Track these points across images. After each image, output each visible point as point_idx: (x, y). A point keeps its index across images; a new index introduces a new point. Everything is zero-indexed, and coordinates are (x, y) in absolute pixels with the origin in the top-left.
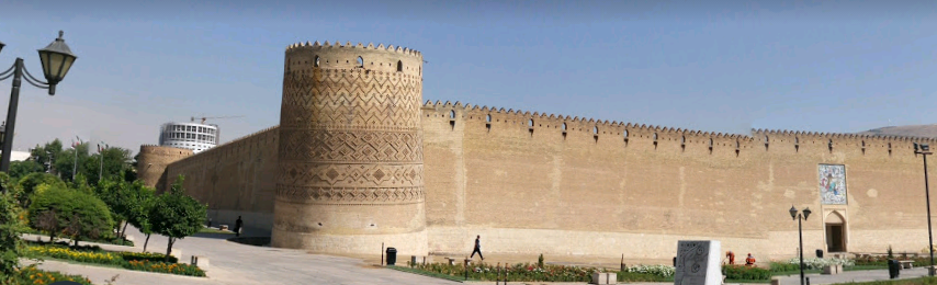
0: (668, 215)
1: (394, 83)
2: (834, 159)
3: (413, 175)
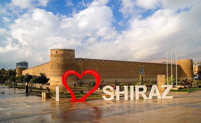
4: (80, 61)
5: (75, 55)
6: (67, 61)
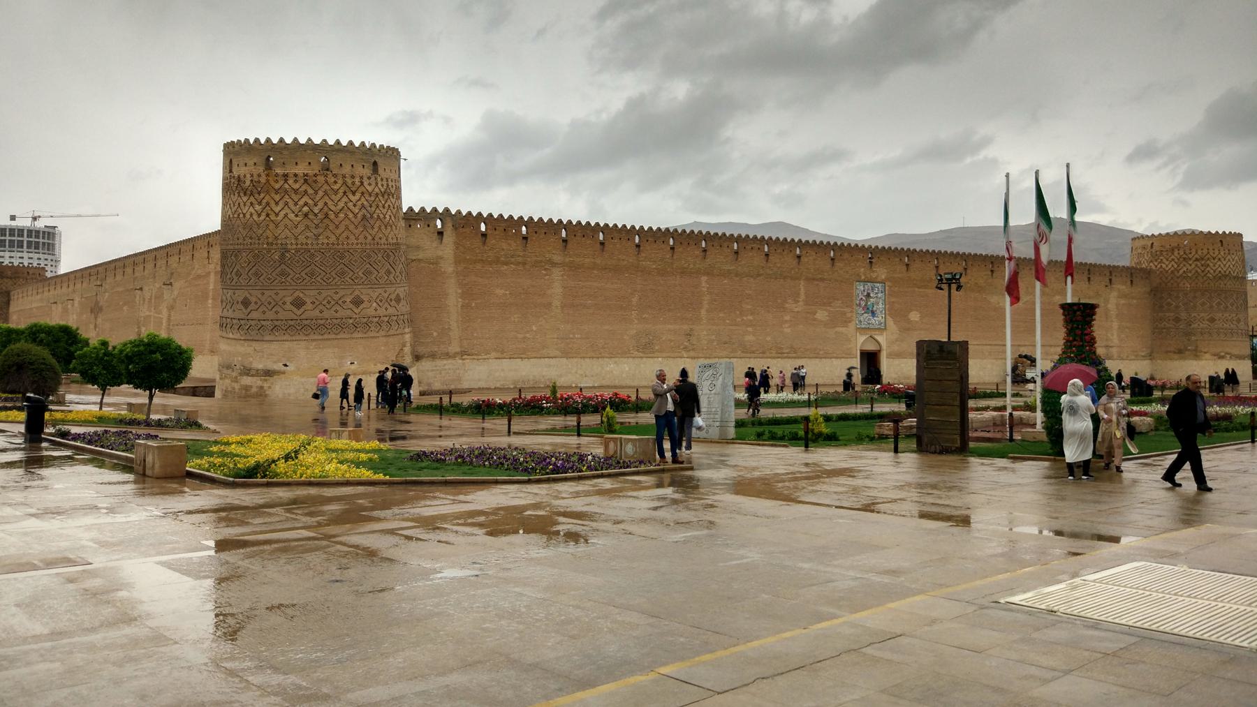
0: (689, 335)
1: (370, 189)
2: (874, 275)
3: (398, 300)
4: (440, 233)
5: (398, 189)
6: (342, 228)
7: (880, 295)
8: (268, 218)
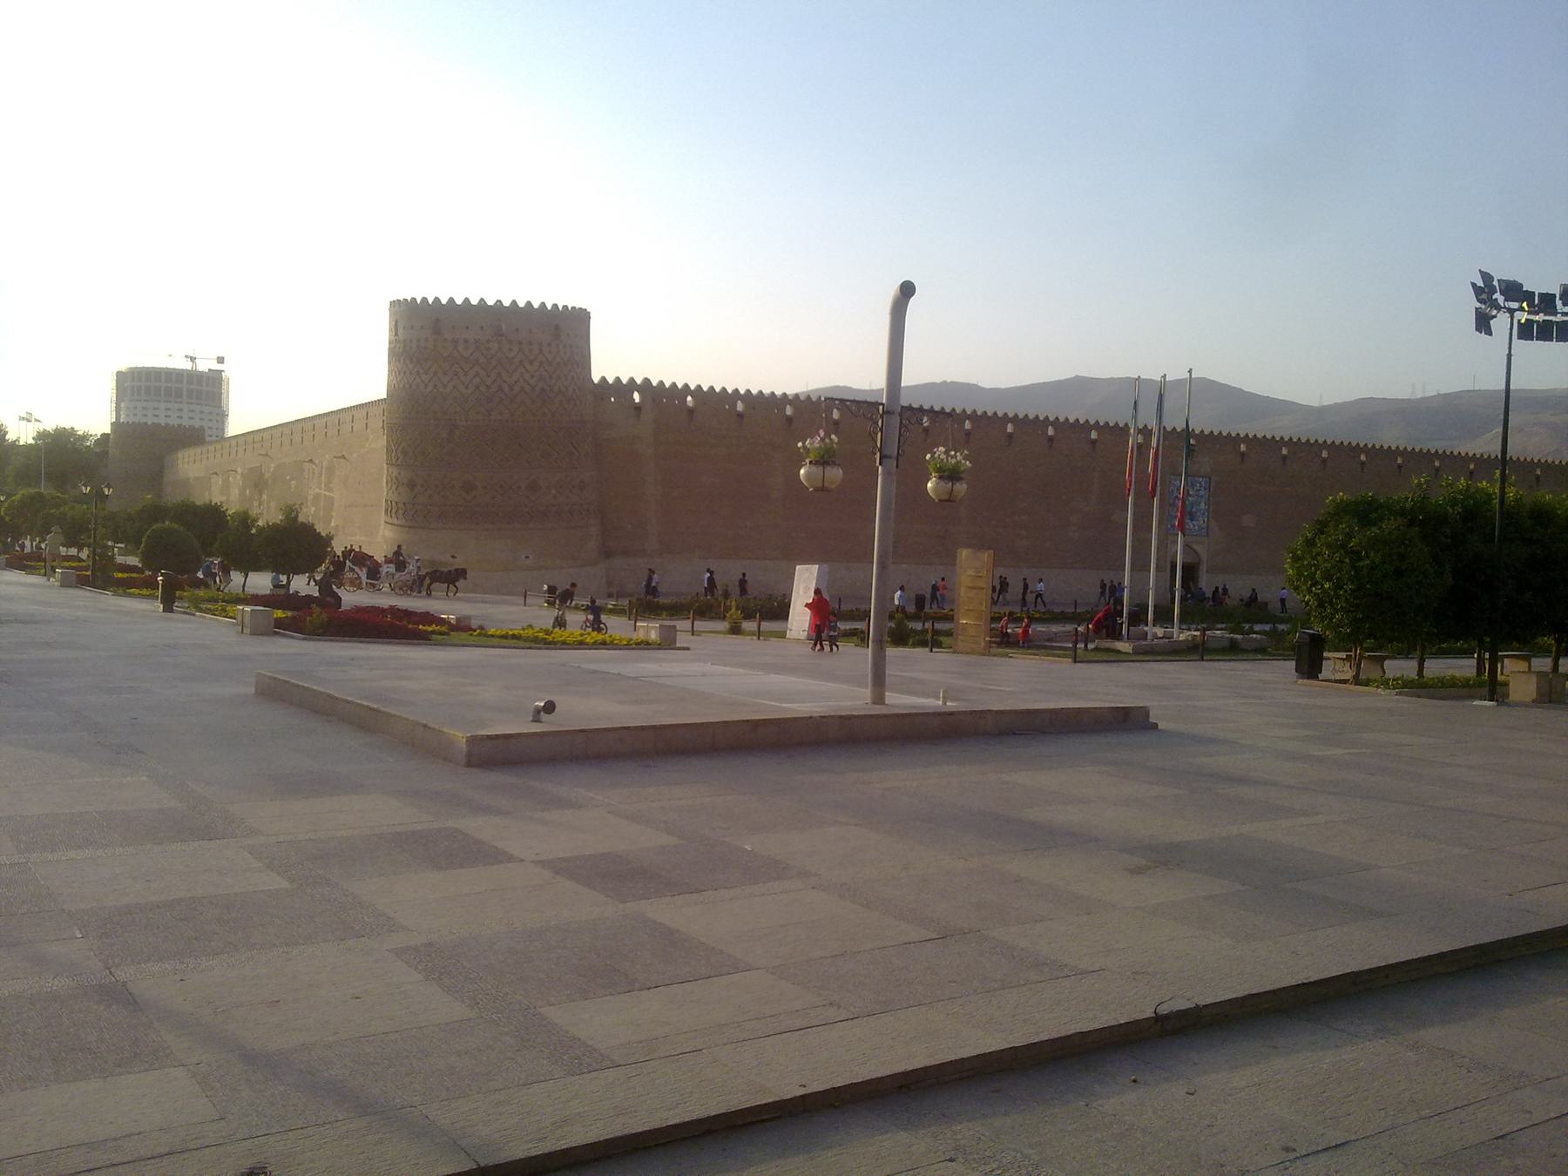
7: (1202, 493)
8: (435, 390)
